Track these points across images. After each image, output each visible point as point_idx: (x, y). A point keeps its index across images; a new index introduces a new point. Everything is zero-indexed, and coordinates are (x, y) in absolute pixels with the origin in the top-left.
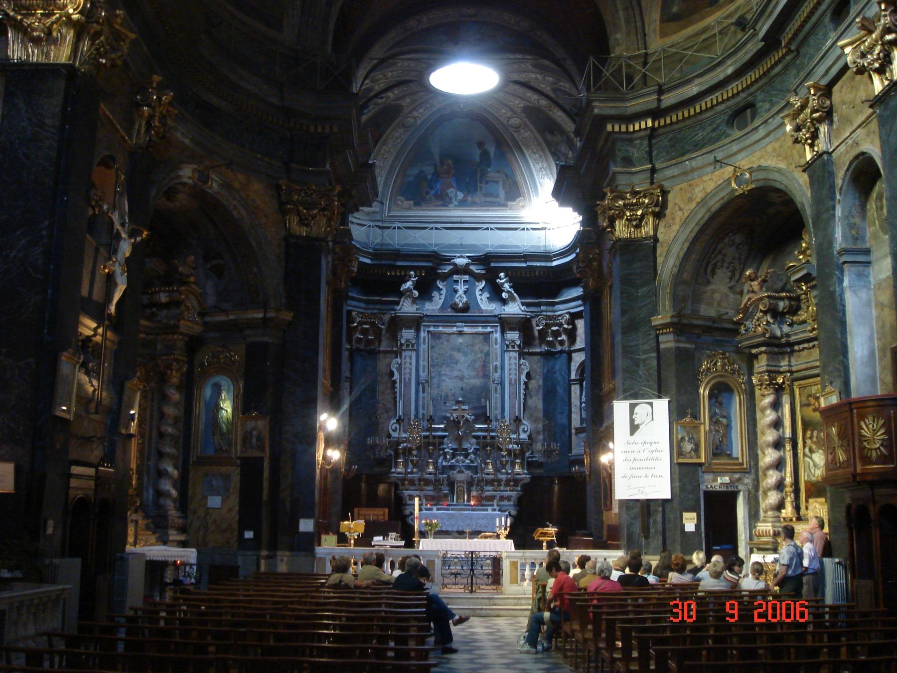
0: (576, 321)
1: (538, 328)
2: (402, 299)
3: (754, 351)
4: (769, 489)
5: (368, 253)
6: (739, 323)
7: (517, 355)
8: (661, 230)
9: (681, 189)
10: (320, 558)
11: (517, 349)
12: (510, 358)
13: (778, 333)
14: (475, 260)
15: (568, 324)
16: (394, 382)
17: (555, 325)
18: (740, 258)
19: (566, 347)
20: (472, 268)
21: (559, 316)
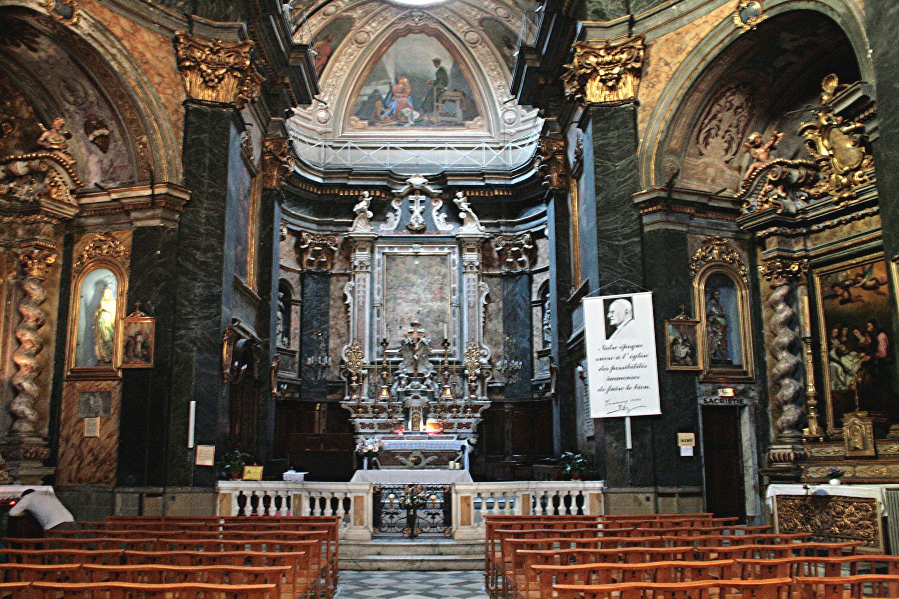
0: (537, 241)
1: (498, 249)
2: (356, 220)
3: (760, 234)
4: (786, 403)
5: (319, 171)
6: (739, 202)
7: (475, 277)
8: (643, 90)
9: (667, 40)
10: (225, 495)
11: (475, 270)
12: (469, 279)
13: (793, 210)
14: (432, 180)
15: (529, 244)
16: (348, 306)
17: (515, 246)
18: (737, 127)
19: (527, 268)
20: (429, 188)
21: (520, 236)
